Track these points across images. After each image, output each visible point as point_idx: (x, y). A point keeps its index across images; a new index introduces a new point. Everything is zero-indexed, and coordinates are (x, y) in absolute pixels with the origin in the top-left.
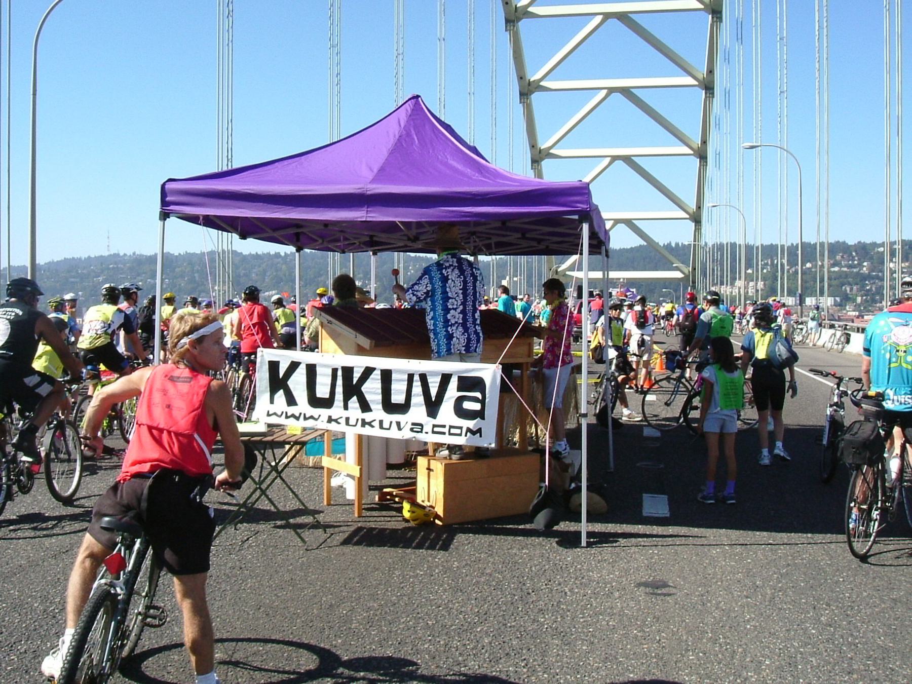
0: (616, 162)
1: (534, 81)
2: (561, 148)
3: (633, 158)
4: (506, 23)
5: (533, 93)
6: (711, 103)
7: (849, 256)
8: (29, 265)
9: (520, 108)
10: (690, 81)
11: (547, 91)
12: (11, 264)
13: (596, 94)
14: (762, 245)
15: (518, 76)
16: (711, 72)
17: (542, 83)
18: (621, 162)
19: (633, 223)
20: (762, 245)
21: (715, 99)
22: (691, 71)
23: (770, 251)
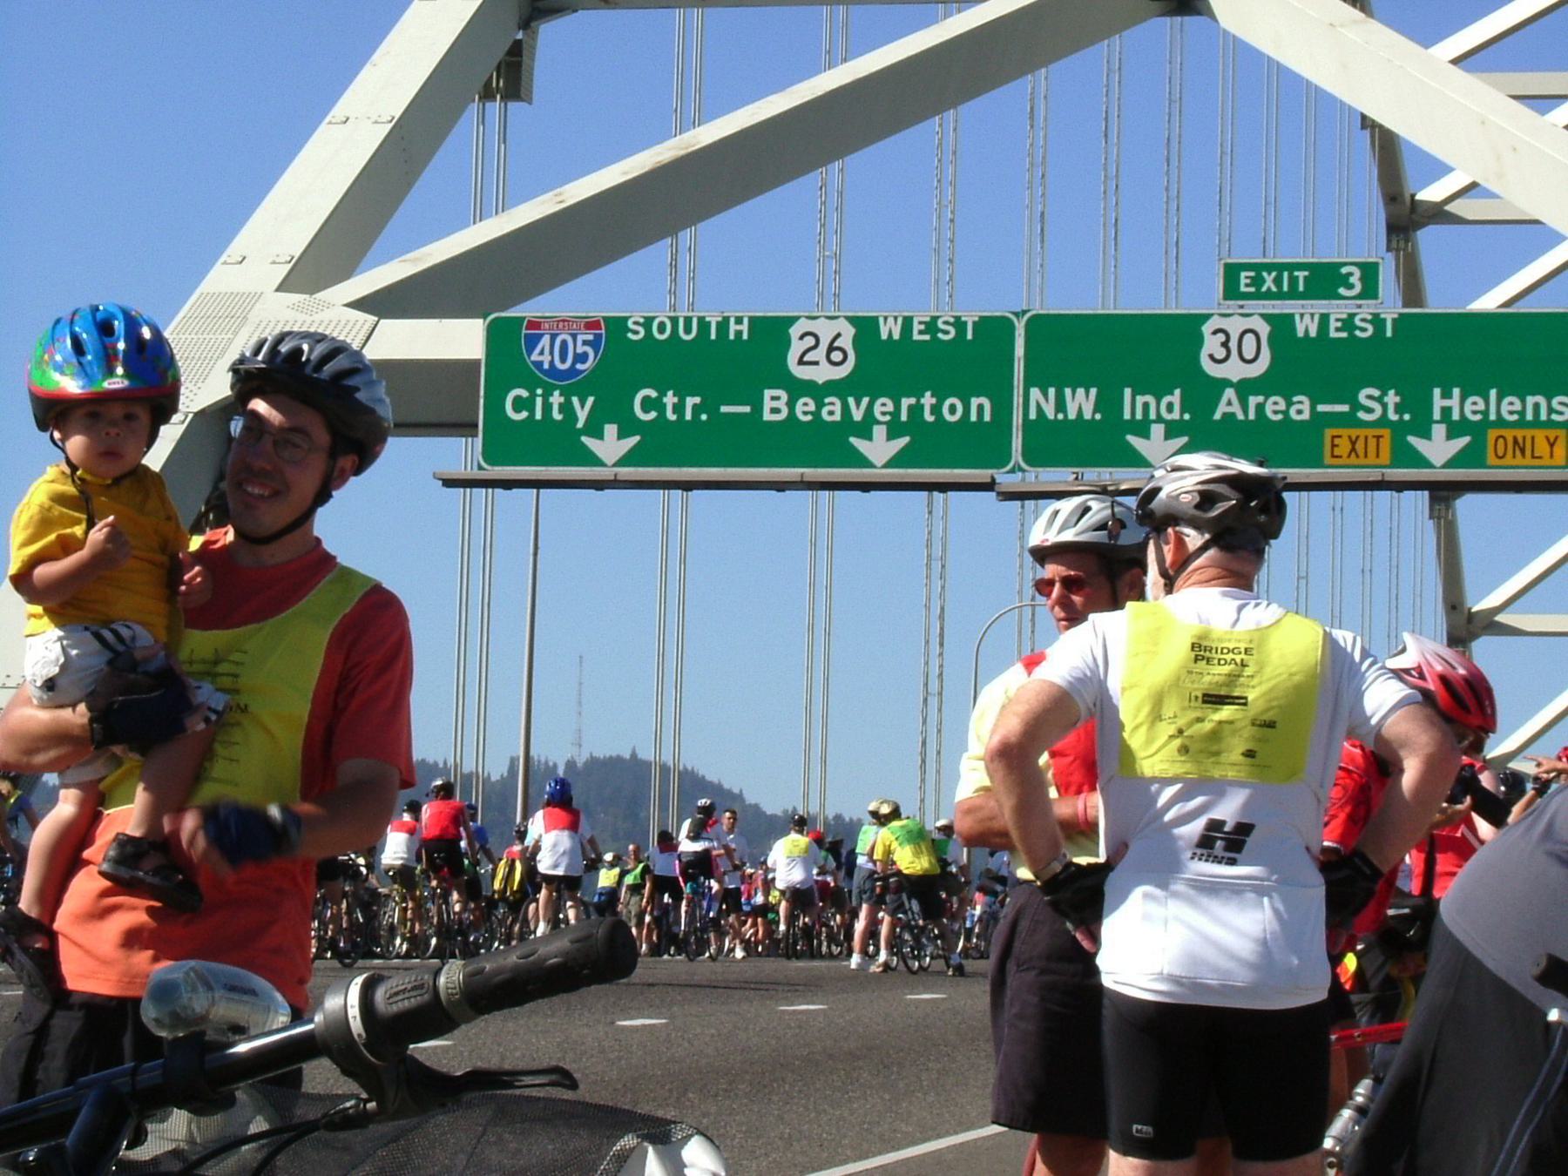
12: (533, 752)
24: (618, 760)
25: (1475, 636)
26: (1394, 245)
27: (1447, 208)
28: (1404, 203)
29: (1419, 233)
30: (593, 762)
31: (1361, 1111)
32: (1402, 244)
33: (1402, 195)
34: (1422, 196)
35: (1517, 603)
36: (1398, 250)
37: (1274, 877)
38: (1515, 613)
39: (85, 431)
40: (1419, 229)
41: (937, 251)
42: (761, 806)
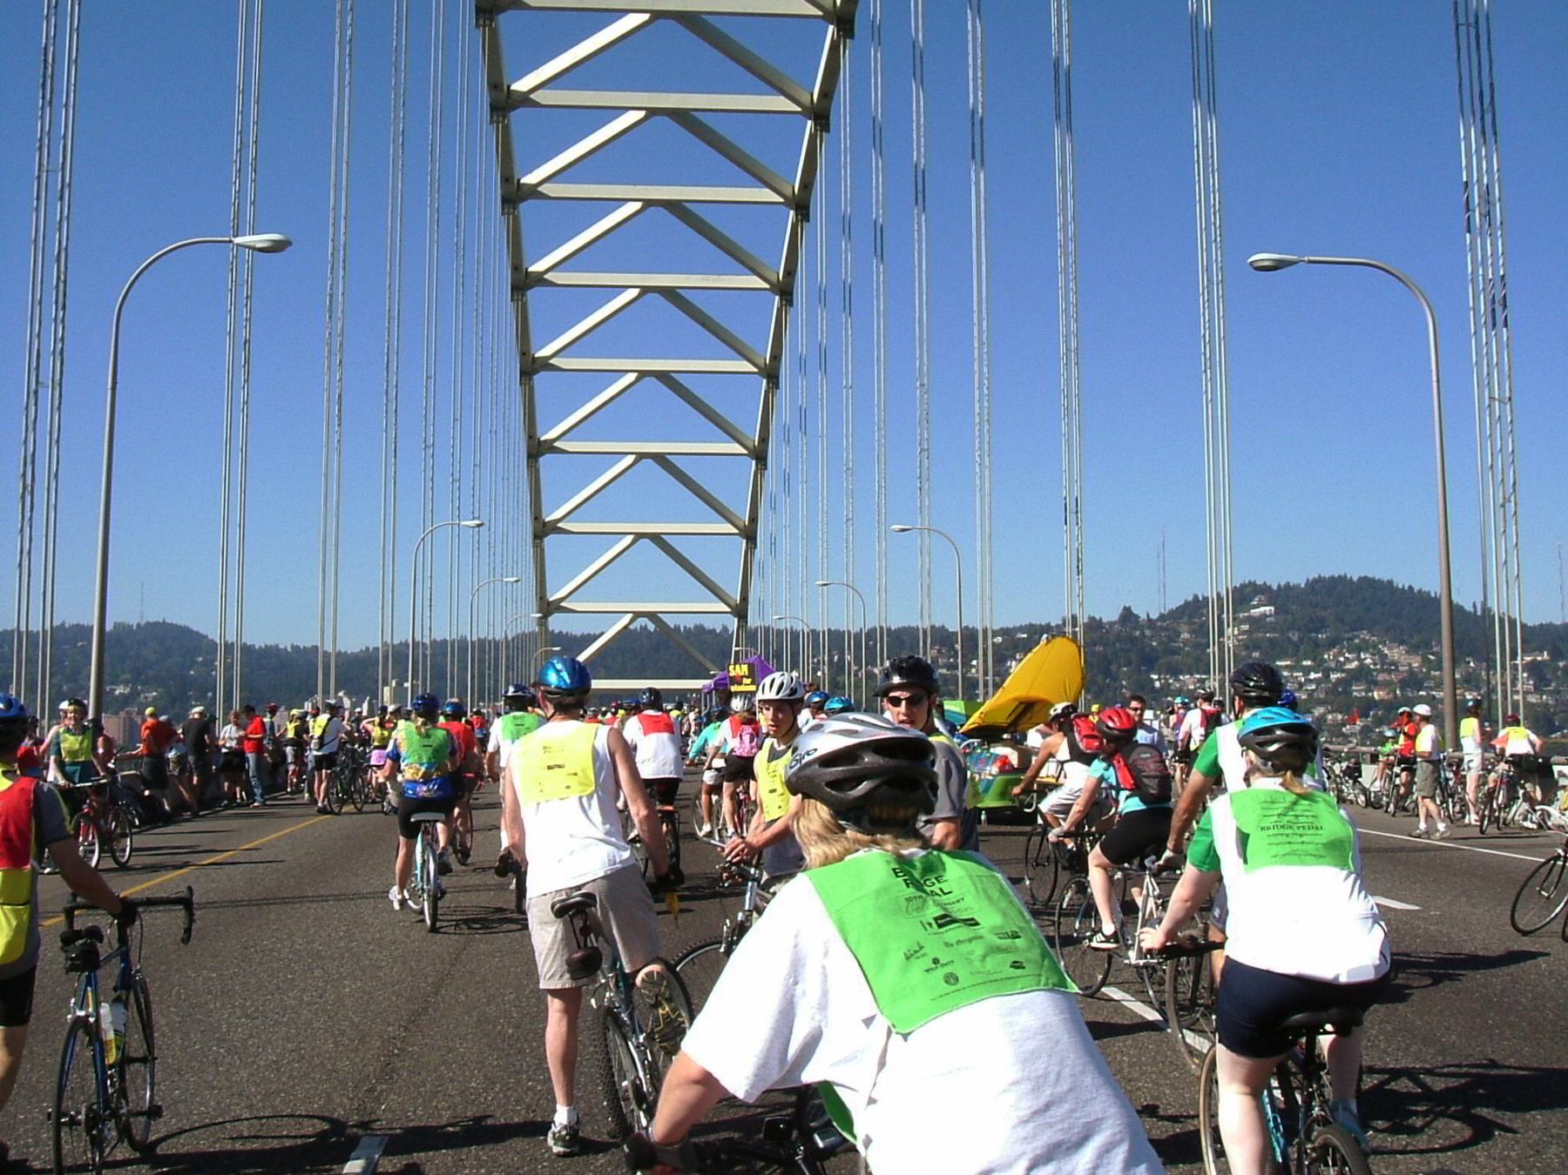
0: (642, 540)
1: (545, 441)
2: (576, 521)
3: (660, 615)
4: (476, 15)
5: (532, 287)
6: (752, 554)
7: (949, 651)
8: (41, 630)
9: (509, 307)
10: (737, 449)
11: (541, 198)
12: (30, 629)
13: (622, 618)
14: (829, 630)
15: (489, 83)
16: (775, 358)
17: (557, 444)
18: (654, 379)
19: (662, 539)
20: (829, 630)
21: (757, 551)
22: (746, 353)
23: (836, 637)
24: (158, 623)
25: (536, 372)
26: (515, 297)
27: (540, 189)
28: (502, 90)
29: (512, 114)
30: (148, 624)
31: (345, 710)
32: (511, 211)
33: (513, 177)
34: (516, 87)
35: (568, 435)
36: (518, 300)
37: (1117, 818)
38: (566, 271)
39: (1351, 686)
40: (500, 13)
41: (233, 335)
42: (1033, 622)
